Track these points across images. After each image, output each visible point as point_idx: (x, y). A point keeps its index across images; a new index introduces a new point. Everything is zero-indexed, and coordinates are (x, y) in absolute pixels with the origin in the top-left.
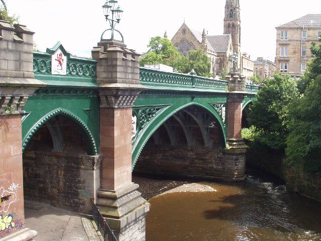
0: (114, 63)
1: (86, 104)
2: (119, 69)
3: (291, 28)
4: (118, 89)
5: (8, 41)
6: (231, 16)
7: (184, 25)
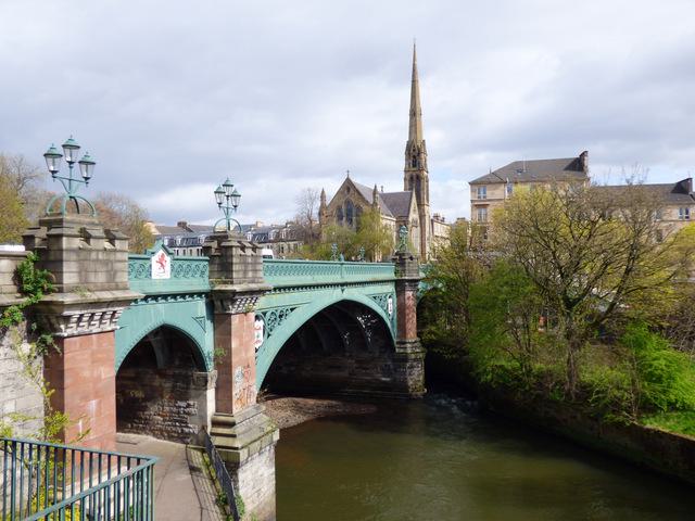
0: (229, 260)
1: (200, 306)
2: (235, 268)
3: (490, 183)
4: (234, 293)
5: (98, 251)
6: (414, 166)
7: (348, 180)
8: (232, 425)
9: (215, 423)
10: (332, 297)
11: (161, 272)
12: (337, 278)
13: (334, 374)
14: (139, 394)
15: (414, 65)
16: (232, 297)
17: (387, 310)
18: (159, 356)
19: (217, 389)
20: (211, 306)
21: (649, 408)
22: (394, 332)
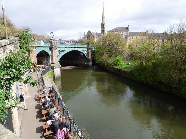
1: (49, 49)
6: (103, 28)
8: (53, 64)
9: (51, 64)
10: (73, 49)
11: (42, 44)
12: (74, 47)
13: (78, 63)
14: (42, 60)
15: (103, 7)
16: (53, 47)
17: (85, 52)
18: (44, 55)
19: (52, 59)
20: (50, 49)
21: (115, 65)
22: (87, 56)
